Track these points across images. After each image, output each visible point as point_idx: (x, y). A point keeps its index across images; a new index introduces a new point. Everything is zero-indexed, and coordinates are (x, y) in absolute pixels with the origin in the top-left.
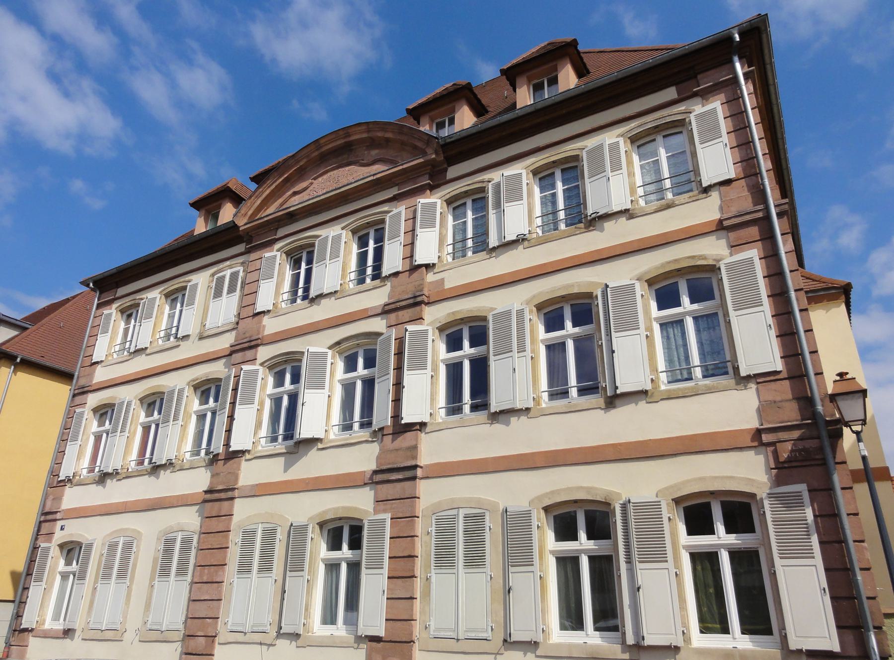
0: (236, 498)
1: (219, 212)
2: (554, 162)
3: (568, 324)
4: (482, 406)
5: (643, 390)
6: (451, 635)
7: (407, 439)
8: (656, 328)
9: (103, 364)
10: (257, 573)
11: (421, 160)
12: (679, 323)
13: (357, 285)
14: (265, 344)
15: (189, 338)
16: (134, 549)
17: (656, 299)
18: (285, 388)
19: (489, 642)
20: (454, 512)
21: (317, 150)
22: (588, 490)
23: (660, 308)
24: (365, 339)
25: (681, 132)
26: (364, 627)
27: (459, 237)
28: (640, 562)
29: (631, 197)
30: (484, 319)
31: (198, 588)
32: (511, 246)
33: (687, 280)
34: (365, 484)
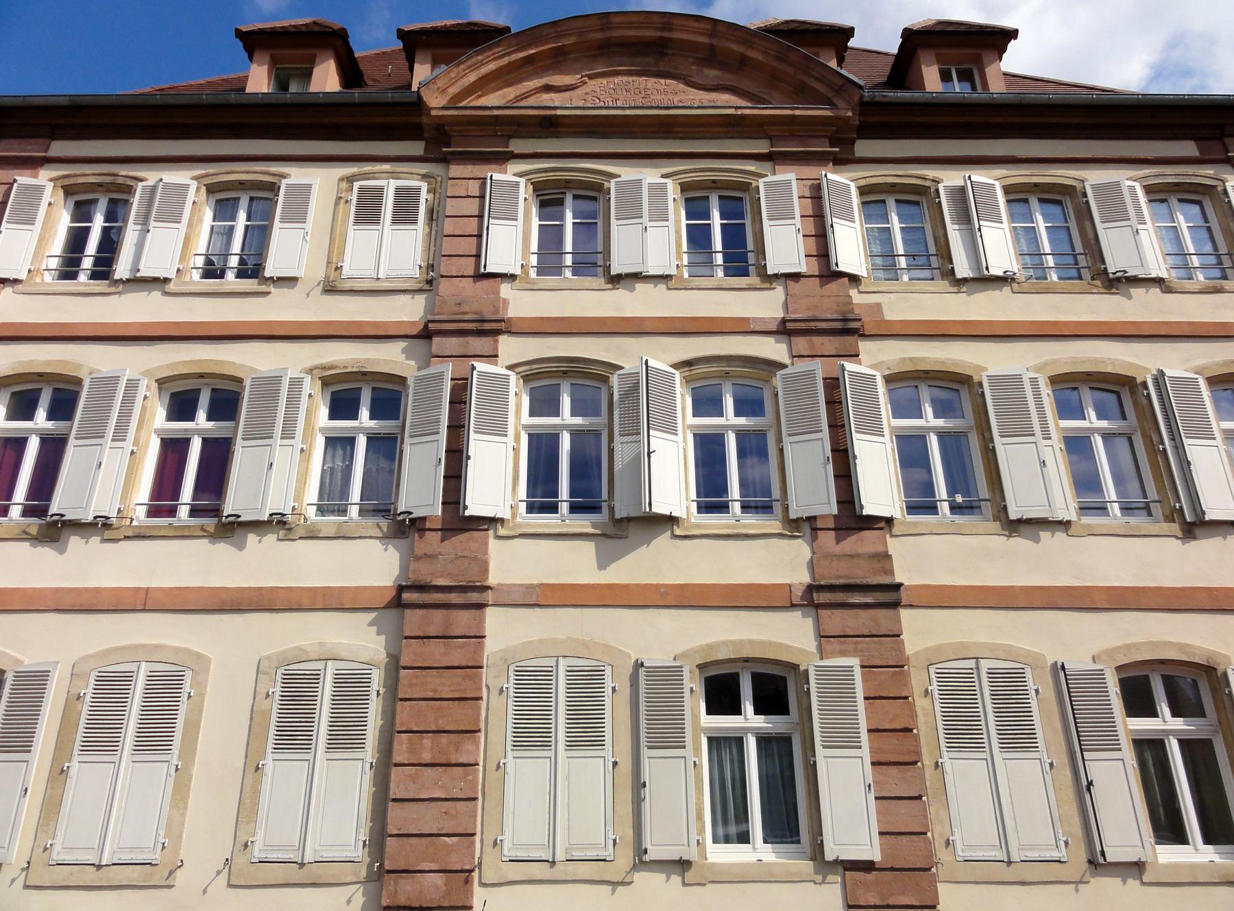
0: (487, 605)
1: (312, 68)
2: (1036, 185)
3: (364, 413)
4: (967, 508)
5: (802, 518)
6: (541, 857)
7: (866, 541)
8: (320, 442)
9: (20, 287)
10: (566, 750)
11: (829, 113)
12: (348, 442)
13: (58, 280)
14: (513, 333)
15: (296, 286)
16: (187, 688)
17: (330, 405)
18: (36, 424)
19: (1064, 864)
20: (320, 665)
21: (601, 30)
22: (1182, 647)
23: (333, 416)
24: (745, 367)
25: (917, 203)
26: (837, 847)
27: (217, 248)
28: (649, 748)
29: (179, 264)
30: (78, 382)
31: (411, 776)
32: (995, 285)
33: (373, 389)
34: (793, 606)
